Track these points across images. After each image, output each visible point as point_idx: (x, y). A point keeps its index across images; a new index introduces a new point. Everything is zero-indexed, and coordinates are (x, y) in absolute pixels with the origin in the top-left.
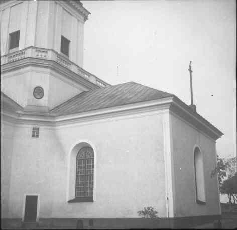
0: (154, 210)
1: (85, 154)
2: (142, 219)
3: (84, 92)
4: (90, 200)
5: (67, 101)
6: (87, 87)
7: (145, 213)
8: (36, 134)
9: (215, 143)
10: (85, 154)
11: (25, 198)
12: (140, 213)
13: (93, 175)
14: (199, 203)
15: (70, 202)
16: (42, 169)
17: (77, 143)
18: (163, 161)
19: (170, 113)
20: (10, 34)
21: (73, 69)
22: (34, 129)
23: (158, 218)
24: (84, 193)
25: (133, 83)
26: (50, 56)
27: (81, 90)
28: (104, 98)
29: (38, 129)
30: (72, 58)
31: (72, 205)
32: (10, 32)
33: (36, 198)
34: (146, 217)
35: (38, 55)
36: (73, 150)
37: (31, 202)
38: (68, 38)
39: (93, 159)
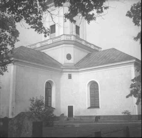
0: (129, 112)
2: (124, 116)
3: (89, 54)
4: (98, 107)
5: (82, 60)
6: (90, 51)
7: (125, 113)
8: (70, 77)
10: (94, 87)
11: (72, 105)
12: (123, 113)
15: (88, 108)
17: (90, 81)
19: (134, 66)
20: (50, 26)
22: (69, 75)
23: (131, 115)
24: (95, 104)
25: (114, 49)
26: (73, 38)
28: (101, 58)
29: (71, 75)
30: (81, 37)
31: (89, 110)
32: (51, 25)
34: (125, 114)
35: (67, 38)
37: (70, 108)
39: (98, 88)
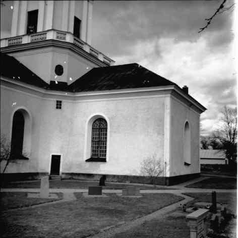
1: (99, 126)
4: (104, 160)
8: (59, 105)
9: (200, 116)
10: (99, 126)
13: (106, 141)
14: (186, 164)
15: (87, 161)
16: (61, 136)
17: (95, 114)
18: (163, 135)
19: (171, 97)
21: (87, 49)
22: (57, 102)
27: (91, 66)
29: (61, 102)
31: (88, 164)
33: (59, 157)
36: (90, 120)
38: (80, 19)
